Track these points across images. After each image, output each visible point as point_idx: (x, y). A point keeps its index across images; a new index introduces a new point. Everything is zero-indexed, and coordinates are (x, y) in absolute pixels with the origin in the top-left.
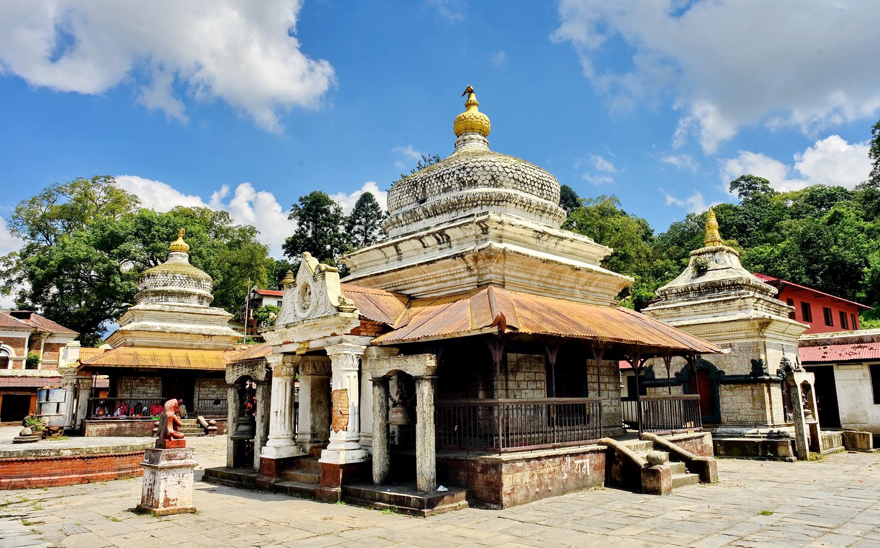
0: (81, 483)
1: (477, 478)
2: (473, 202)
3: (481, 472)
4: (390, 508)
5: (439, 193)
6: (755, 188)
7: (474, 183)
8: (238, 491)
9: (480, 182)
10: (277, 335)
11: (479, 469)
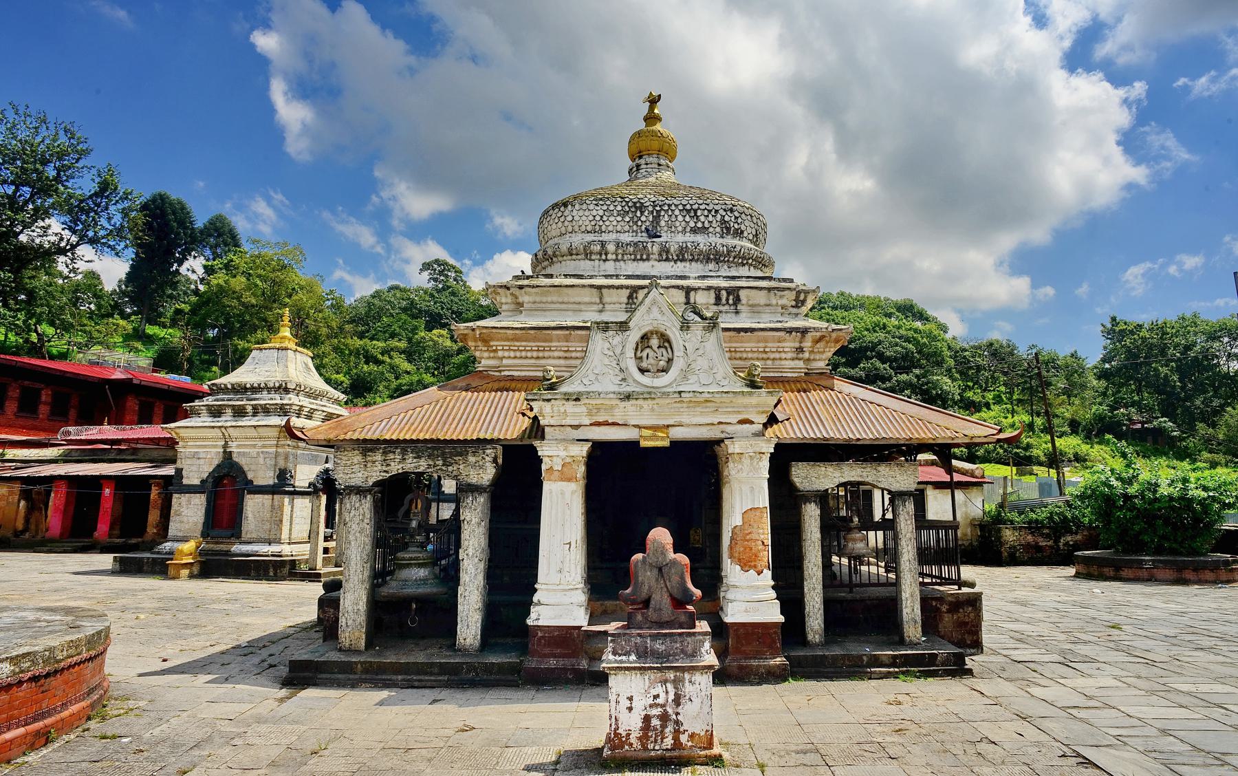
0: (33, 747)
1: (941, 619)
2: (744, 258)
3: (949, 611)
4: (903, 673)
5: (684, 231)
6: (447, 276)
7: (739, 233)
8: (493, 694)
9: (745, 234)
10: (584, 409)
11: (944, 608)
